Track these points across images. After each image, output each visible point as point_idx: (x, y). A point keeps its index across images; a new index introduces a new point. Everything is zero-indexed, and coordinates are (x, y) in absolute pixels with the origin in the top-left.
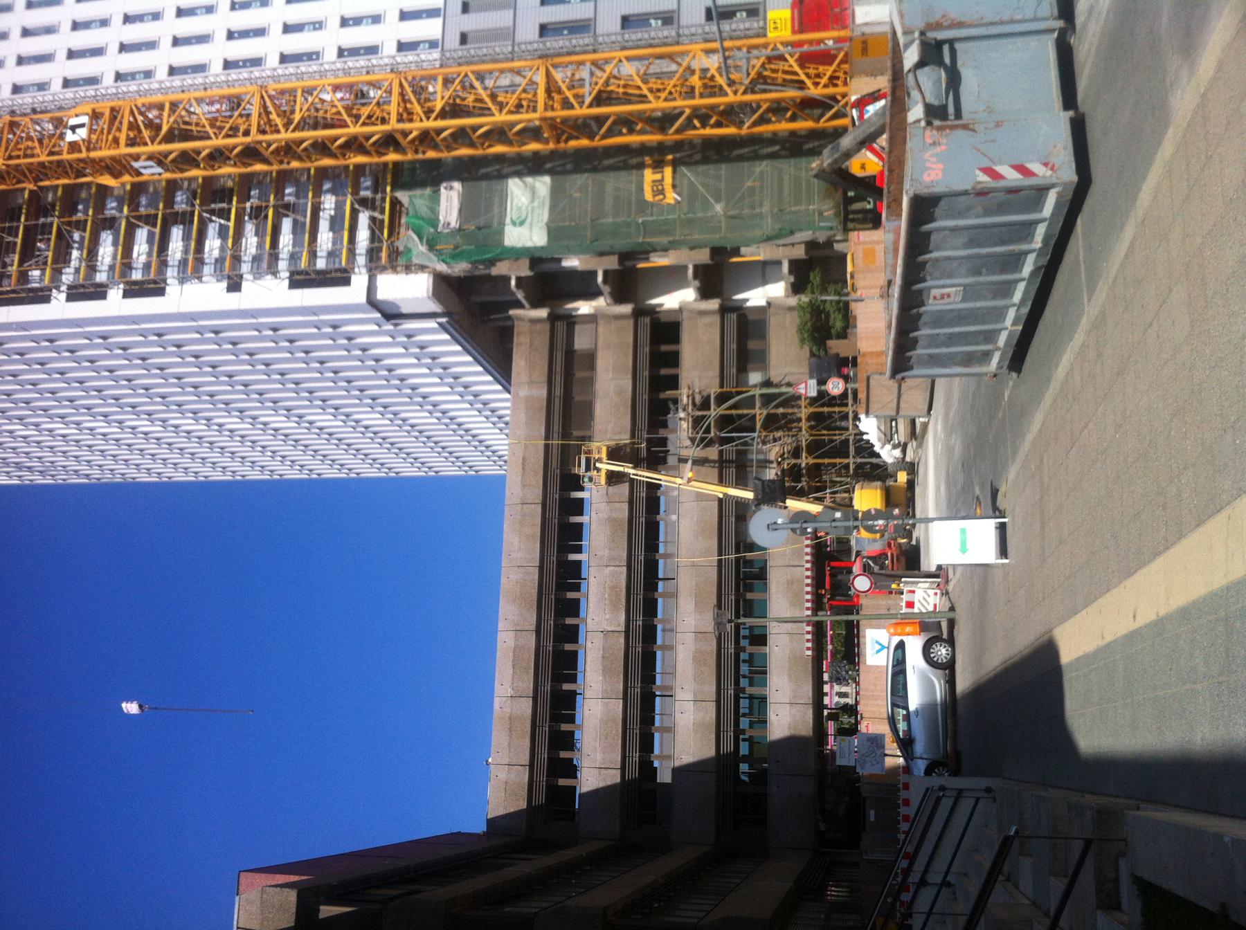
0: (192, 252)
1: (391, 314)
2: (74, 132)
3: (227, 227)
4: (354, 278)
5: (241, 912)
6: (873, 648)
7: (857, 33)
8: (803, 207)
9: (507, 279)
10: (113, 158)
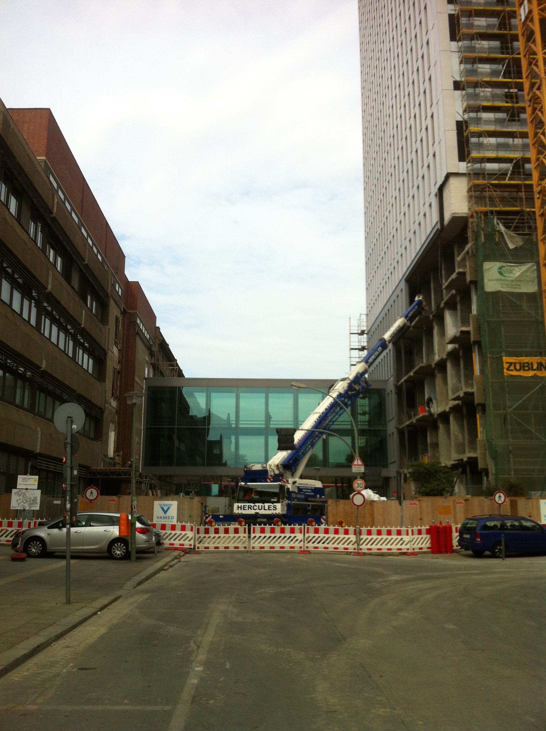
3: (498, 76)
6: (165, 505)
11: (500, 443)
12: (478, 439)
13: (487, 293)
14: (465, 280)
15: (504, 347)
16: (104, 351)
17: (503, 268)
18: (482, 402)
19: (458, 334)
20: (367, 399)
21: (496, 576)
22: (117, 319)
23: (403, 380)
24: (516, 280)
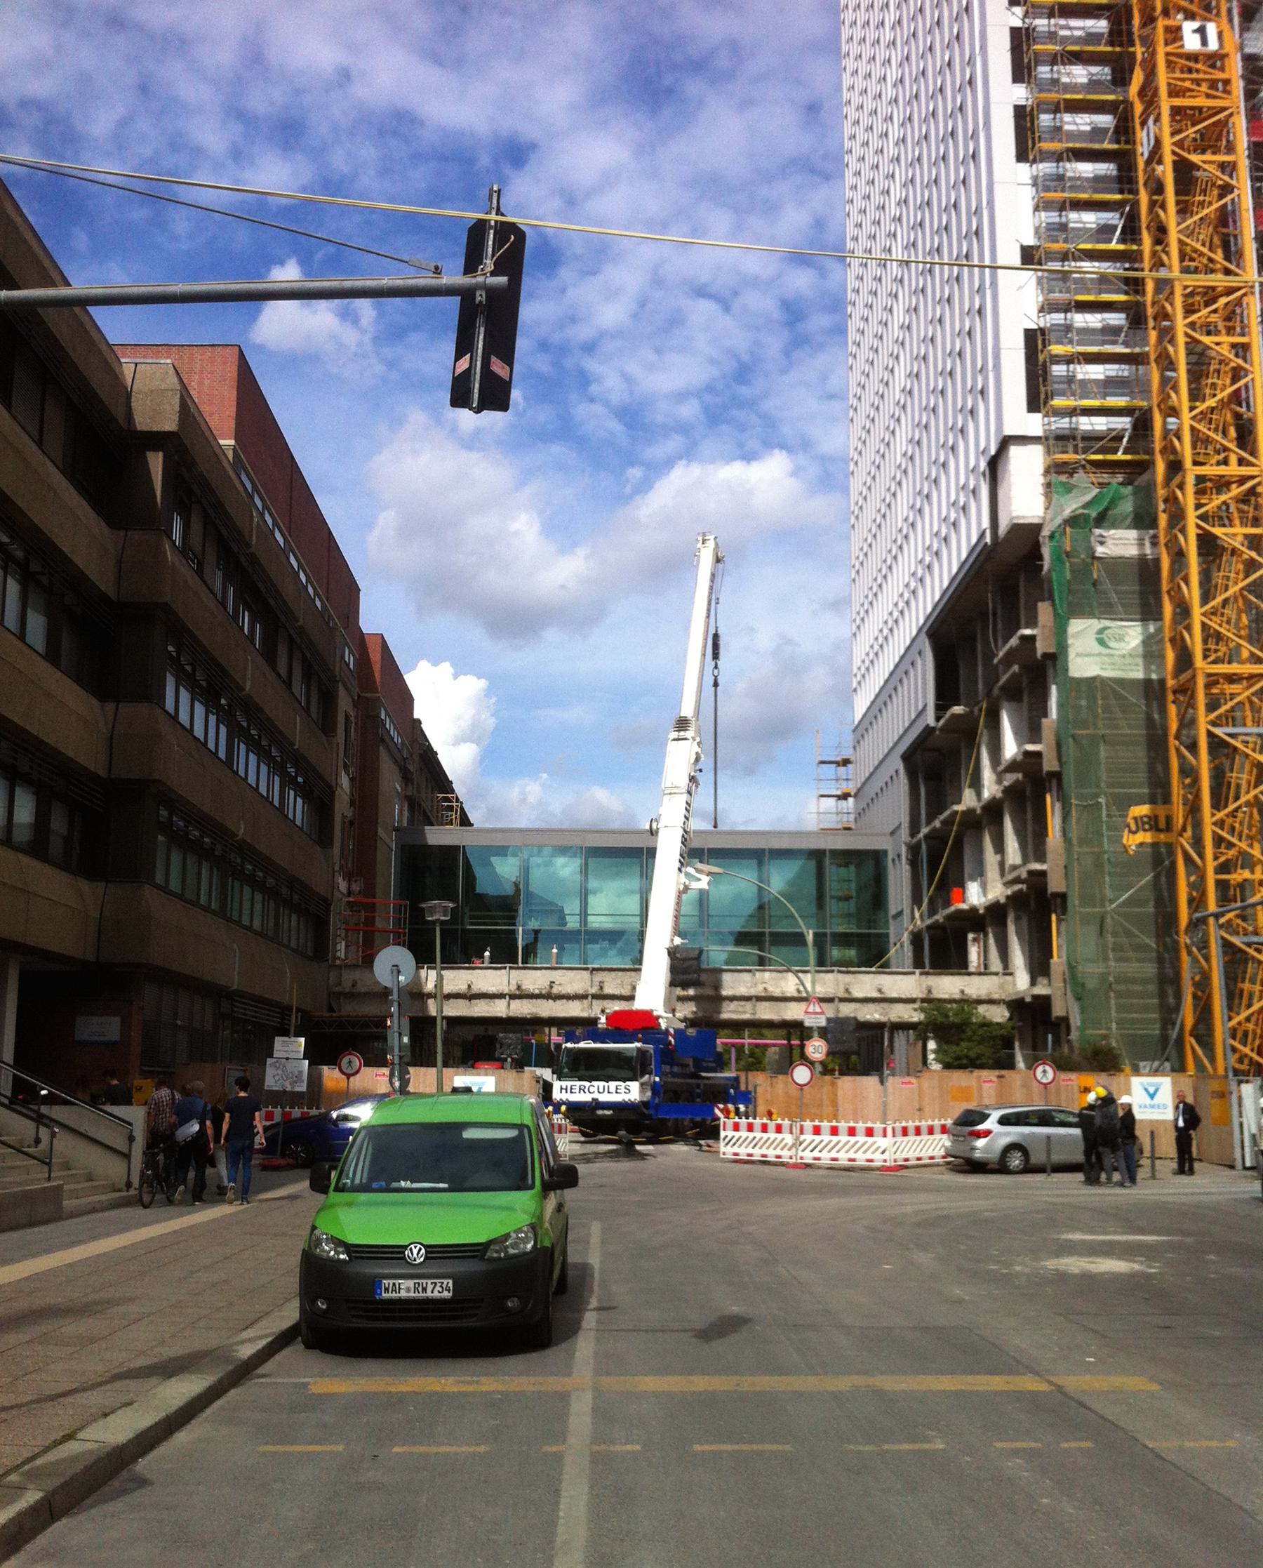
0: (1073, 195)
1: (995, 467)
2: (1195, 31)
4: (1037, 417)
5: (154, 366)
7: (1234, 1087)
8: (1114, 1014)
9: (1033, 623)
10: (1156, 91)
11: (1091, 971)
12: (1052, 961)
13: (1074, 679)
14: (1035, 649)
15: (1103, 785)
16: (330, 787)
17: (1106, 632)
18: (1062, 889)
19: (1020, 758)
20: (852, 868)
21: (309, 944)
22: (347, 717)
23: (921, 835)
24: (1130, 655)
